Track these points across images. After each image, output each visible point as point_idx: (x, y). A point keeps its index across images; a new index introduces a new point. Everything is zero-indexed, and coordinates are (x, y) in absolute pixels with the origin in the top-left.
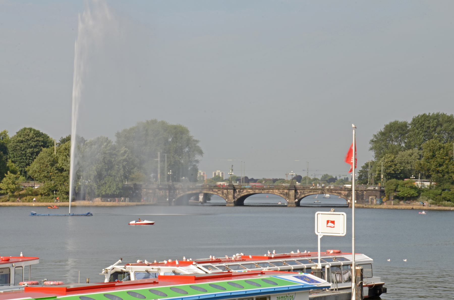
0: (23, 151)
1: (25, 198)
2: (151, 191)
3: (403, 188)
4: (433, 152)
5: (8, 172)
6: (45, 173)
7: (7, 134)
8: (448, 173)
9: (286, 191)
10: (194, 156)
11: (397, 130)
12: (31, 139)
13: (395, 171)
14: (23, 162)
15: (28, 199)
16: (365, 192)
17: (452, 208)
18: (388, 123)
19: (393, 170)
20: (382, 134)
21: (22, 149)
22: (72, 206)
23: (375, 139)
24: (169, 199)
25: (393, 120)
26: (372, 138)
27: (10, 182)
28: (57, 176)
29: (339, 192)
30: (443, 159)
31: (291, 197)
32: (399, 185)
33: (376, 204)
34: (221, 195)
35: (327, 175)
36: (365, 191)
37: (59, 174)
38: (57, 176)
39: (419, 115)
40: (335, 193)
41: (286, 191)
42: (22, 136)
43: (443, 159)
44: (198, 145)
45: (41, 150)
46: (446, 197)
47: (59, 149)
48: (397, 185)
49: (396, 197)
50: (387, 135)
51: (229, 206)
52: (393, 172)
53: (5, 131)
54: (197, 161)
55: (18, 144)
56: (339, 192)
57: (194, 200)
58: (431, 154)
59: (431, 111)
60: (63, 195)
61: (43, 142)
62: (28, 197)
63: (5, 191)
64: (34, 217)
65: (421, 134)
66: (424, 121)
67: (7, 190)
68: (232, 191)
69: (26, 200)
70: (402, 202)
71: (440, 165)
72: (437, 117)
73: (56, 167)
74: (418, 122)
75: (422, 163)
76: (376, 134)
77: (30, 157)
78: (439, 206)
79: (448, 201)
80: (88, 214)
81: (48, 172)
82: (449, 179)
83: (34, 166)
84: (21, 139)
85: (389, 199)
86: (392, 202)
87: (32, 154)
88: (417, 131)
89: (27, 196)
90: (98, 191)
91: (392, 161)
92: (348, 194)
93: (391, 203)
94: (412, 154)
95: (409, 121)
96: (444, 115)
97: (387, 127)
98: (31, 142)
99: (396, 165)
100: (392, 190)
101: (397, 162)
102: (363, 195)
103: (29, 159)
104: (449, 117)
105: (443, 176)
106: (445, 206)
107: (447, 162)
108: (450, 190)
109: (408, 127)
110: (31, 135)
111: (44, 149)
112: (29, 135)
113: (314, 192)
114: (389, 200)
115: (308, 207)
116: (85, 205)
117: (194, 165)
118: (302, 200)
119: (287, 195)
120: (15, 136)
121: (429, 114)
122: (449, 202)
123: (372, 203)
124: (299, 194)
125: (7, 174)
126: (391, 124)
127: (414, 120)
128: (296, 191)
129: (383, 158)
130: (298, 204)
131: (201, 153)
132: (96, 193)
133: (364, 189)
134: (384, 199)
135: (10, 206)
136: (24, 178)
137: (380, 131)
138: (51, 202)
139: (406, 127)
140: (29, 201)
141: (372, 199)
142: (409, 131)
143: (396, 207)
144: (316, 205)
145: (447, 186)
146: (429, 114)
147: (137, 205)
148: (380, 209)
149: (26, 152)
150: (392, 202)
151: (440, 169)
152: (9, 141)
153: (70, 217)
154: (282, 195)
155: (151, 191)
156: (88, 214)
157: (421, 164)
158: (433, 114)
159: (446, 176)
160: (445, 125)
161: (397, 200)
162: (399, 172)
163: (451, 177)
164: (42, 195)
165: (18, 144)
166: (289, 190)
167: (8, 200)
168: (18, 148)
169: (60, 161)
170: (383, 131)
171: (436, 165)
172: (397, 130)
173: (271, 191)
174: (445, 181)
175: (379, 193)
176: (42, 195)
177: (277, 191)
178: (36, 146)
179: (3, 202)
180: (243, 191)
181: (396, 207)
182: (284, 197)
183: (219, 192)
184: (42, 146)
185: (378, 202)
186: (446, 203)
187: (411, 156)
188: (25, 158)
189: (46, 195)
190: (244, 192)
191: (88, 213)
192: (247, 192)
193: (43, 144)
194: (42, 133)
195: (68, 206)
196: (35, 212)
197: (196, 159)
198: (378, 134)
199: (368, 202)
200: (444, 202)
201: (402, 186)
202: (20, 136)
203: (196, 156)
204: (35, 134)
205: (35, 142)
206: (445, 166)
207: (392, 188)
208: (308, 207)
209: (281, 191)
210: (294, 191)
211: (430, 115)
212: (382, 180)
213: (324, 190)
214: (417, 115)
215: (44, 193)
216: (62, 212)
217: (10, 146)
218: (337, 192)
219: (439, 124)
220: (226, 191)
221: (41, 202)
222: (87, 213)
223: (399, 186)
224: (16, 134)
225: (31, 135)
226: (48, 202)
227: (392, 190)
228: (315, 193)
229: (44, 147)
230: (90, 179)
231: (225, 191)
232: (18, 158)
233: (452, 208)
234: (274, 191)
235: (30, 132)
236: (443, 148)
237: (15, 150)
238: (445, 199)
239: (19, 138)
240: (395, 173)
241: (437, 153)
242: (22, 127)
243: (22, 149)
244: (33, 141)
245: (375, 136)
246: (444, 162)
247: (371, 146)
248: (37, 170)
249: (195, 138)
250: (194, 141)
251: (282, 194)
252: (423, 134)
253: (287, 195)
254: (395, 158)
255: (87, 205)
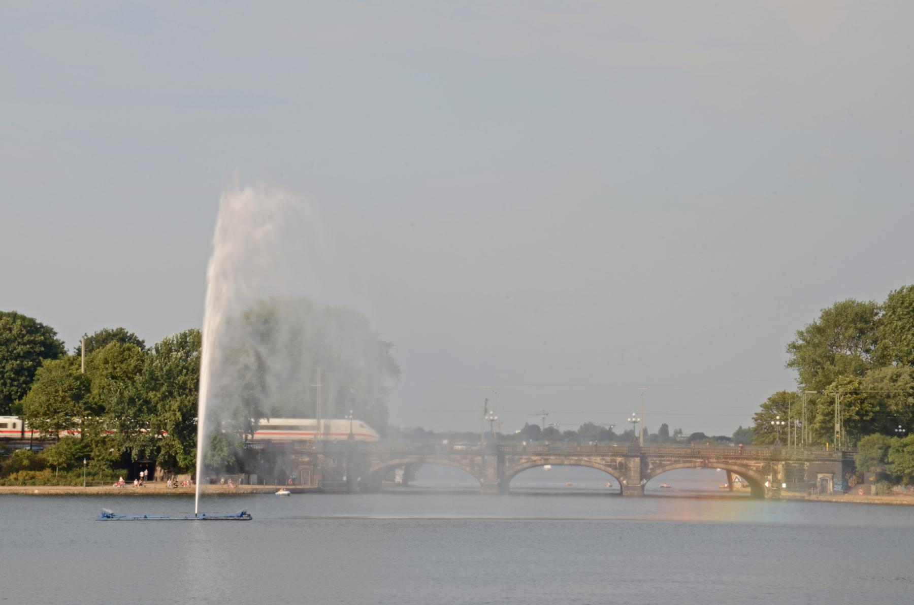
1: (12, 476)
9: (619, 459)
11: (853, 321)
12: (16, 339)
15: (20, 479)
16: (807, 464)
19: (858, 413)
20: (818, 330)
22: (203, 496)
25: (842, 299)
26: (794, 338)
31: (632, 474)
32: (890, 447)
33: (835, 493)
34: (468, 469)
35: (591, 424)
36: (807, 460)
39: (903, 289)
40: (735, 464)
47: (92, 361)
48: (886, 448)
49: (885, 477)
52: (857, 418)
56: (745, 462)
60: (104, 467)
61: (43, 344)
62: (22, 474)
64: (110, 523)
65: (909, 330)
68: (492, 459)
70: (897, 489)
73: (85, 403)
74: (903, 303)
76: (803, 329)
77: (13, 380)
85: (861, 480)
86: (873, 488)
87: (18, 372)
89: (17, 471)
90: (185, 459)
92: (764, 468)
93: (869, 489)
95: (881, 300)
97: (827, 314)
98: (15, 345)
100: (873, 459)
101: (865, 395)
102: (802, 470)
103: (12, 385)
109: (877, 314)
110: (15, 332)
111: (47, 362)
112: (10, 330)
113: (685, 462)
114: (862, 482)
116: (157, 491)
123: (824, 490)
124: (651, 466)
127: (891, 298)
128: (643, 458)
129: (834, 384)
133: (805, 457)
137: (812, 323)
138: (76, 485)
140: (24, 484)
141: (823, 480)
148: (887, 504)
153: (196, 524)
154: (610, 469)
155: (306, 459)
156: (244, 517)
162: (868, 418)
164: (53, 468)
166: (627, 456)
170: (819, 322)
172: (853, 321)
173: (586, 459)
176: (53, 468)
177: (598, 459)
178: (28, 355)
181: (887, 499)
182: (616, 474)
183: (464, 461)
184: (40, 354)
185: (839, 488)
187: (895, 381)
189: (63, 469)
190: (523, 461)
191: (243, 514)
193: (42, 349)
194: (41, 324)
195: (192, 496)
196: (110, 512)
199: (815, 486)
201: (898, 451)
204: (24, 327)
205: (24, 344)
207: (874, 455)
210: (637, 460)
213: (708, 458)
215: (59, 464)
216: (177, 509)
218: (738, 462)
220: (480, 458)
221: (53, 485)
222: (239, 512)
223: (890, 451)
225: (15, 332)
226: (70, 485)
227: (873, 459)
229: (45, 358)
230: (167, 431)
231: (478, 459)
234: (593, 458)
235: (14, 322)
244: (19, 344)
248: (42, 411)
251: (610, 466)
255: (162, 492)
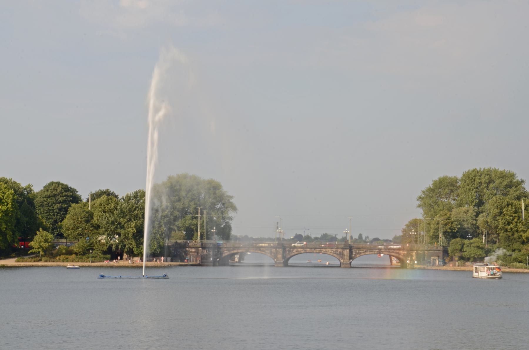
0: (50, 206)
1: (58, 258)
2: (193, 250)
3: (469, 248)
4: (501, 209)
5: (41, 229)
6: (80, 231)
7: (32, 188)
8: (517, 231)
9: (339, 250)
10: (227, 213)
13: (452, 230)
14: (51, 219)
15: (61, 259)
17: (526, 271)
18: (436, 178)
19: (450, 228)
20: (431, 190)
21: (50, 204)
23: (423, 196)
24: (214, 259)
26: (420, 194)
27: (43, 240)
28: (93, 234)
29: (398, 251)
30: (512, 216)
31: (346, 257)
33: (439, 265)
35: (326, 234)
37: (95, 231)
38: (93, 234)
40: (393, 252)
41: (339, 250)
42: (50, 191)
43: (512, 216)
44: (231, 201)
45: (70, 206)
46: (517, 258)
49: (462, 258)
50: (437, 191)
51: (277, 266)
52: (449, 230)
53: (29, 185)
54: (230, 218)
55: (45, 199)
56: (398, 251)
57: (453, 266)
58: (499, 211)
59: (482, 165)
61: (71, 196)
62: (62, 257)
63: (37, 250)
66: (474, 176)
67: (39, 248)
68: (281, 250)
69: (59, 259)
70: (468, 263)
71: (509, 224)
72: (488, 172)
75: (489, 220)
77: (58, 213)
78: (509, 268)
79: (519, 262)
80: (165, 277)
81: (82, 229)
82: (519, 238)
83: (67, 222)
84: (49, 193)
85: (452, 260)
86: (457, 263)
87: (60, 209)
88: (468, 187)
90: (137, 250)
91: (449, 219)
92: (406, 254)
93: (455, 264)
94: (468, 211)
95: (460, 176)
96: (495, 170)
97: (435, 182)
99: (452, 223)
100: (457, 250)
102: (424, 255)
103: (57, 216)
104: (501, 173)
105: (513, 235)
106: (517, 268)
107: (516, 220)
108: (520, 251)
111: (73, 205)
112: (57, 190)
113: (370, 251)
114: (452, 261)
115: (370, 268)
117: (227, 223)
118: (291, 259)
119: (342, 255)
120: (42, 190)
121: (481, 169)
122: (521, 264)
123: (434, 264)
124: (354, 253)
125: (39, 231)
126: (440, 179)
127: (464, 175)
130: (286, 264)
131: (234, 209)
132: (135, 252)
134: (447, 259)
135: (42, 266)
136: (52, 235)
138: (87, 262)
139: (457, 182)
140: (63, 261)
141: (434, 259)
142: (459, 187)
143: (463, 268)
144: (376, 266)
145: (516, 246)
146: (481, 169)
147: (181, 265)
149: (53, 207)
150: (457, 263)
151: (509, 227)
152: (35, 196)
154: (335, 255)
156: (165, 277)
157: (487, 222)
158: (484, 169)
159: (516, 235)
160: (497, 181)
161: (462, 261)
163: (521, 236)
164: (76, 254)
165: (45, 199)
167: (40, 260)
168: (46, 203)
169: (95, 218)
171: (505, 223)
174: (514, 241)
175: (442, 253)
176: (76, 254)
178: (64, 202)
179: (34, 261)
180: (293, 251)
181: (463, 268)
183: (267, 251)
184: (70, 201)
185: (441, 263)
186: (518, 264)
188: (52, 214)
189: (81, 254)
192: (297, 251)
195: (142, 267)
197: (230, 215)
198: (426, 191)
199: (430, 262)
200: (515, 264)
201: (468, 246)
202: (48, 191)
203: (229, 212)
205: (63, 197)
206: (514, 224)
207: (457, 248)
208: (370, 268)
209: (334, 250)
210: (348, 250)
211: (482, 170)
212: (440, 239)
214: (467, 171)
215: (79, 252)
217: (37, 201)
219: (491, 181)
223: (465, 246)
224: (43, 189)
227: (457, 250)
228: (371, 253)
229: (72, 203)
232: (45, 214)
233: (526, 271)
234: (327, 250)
235: (59, 186)
236: (512, 204)
237: (42, 205)
238: (516, 260)
239: (46, 193)
240: (452, 232)
241: (504, 210)
242: (49, 181)
243: (50, 204)
245: (423, 192)
246: (513, 219)
247: (419, 202)
248: (71, 227)
249: (229, 194)
250: (228, 196)
251: (335, 253)
252: (475, 190)
253: (342, 255)
254: (450, 215)
